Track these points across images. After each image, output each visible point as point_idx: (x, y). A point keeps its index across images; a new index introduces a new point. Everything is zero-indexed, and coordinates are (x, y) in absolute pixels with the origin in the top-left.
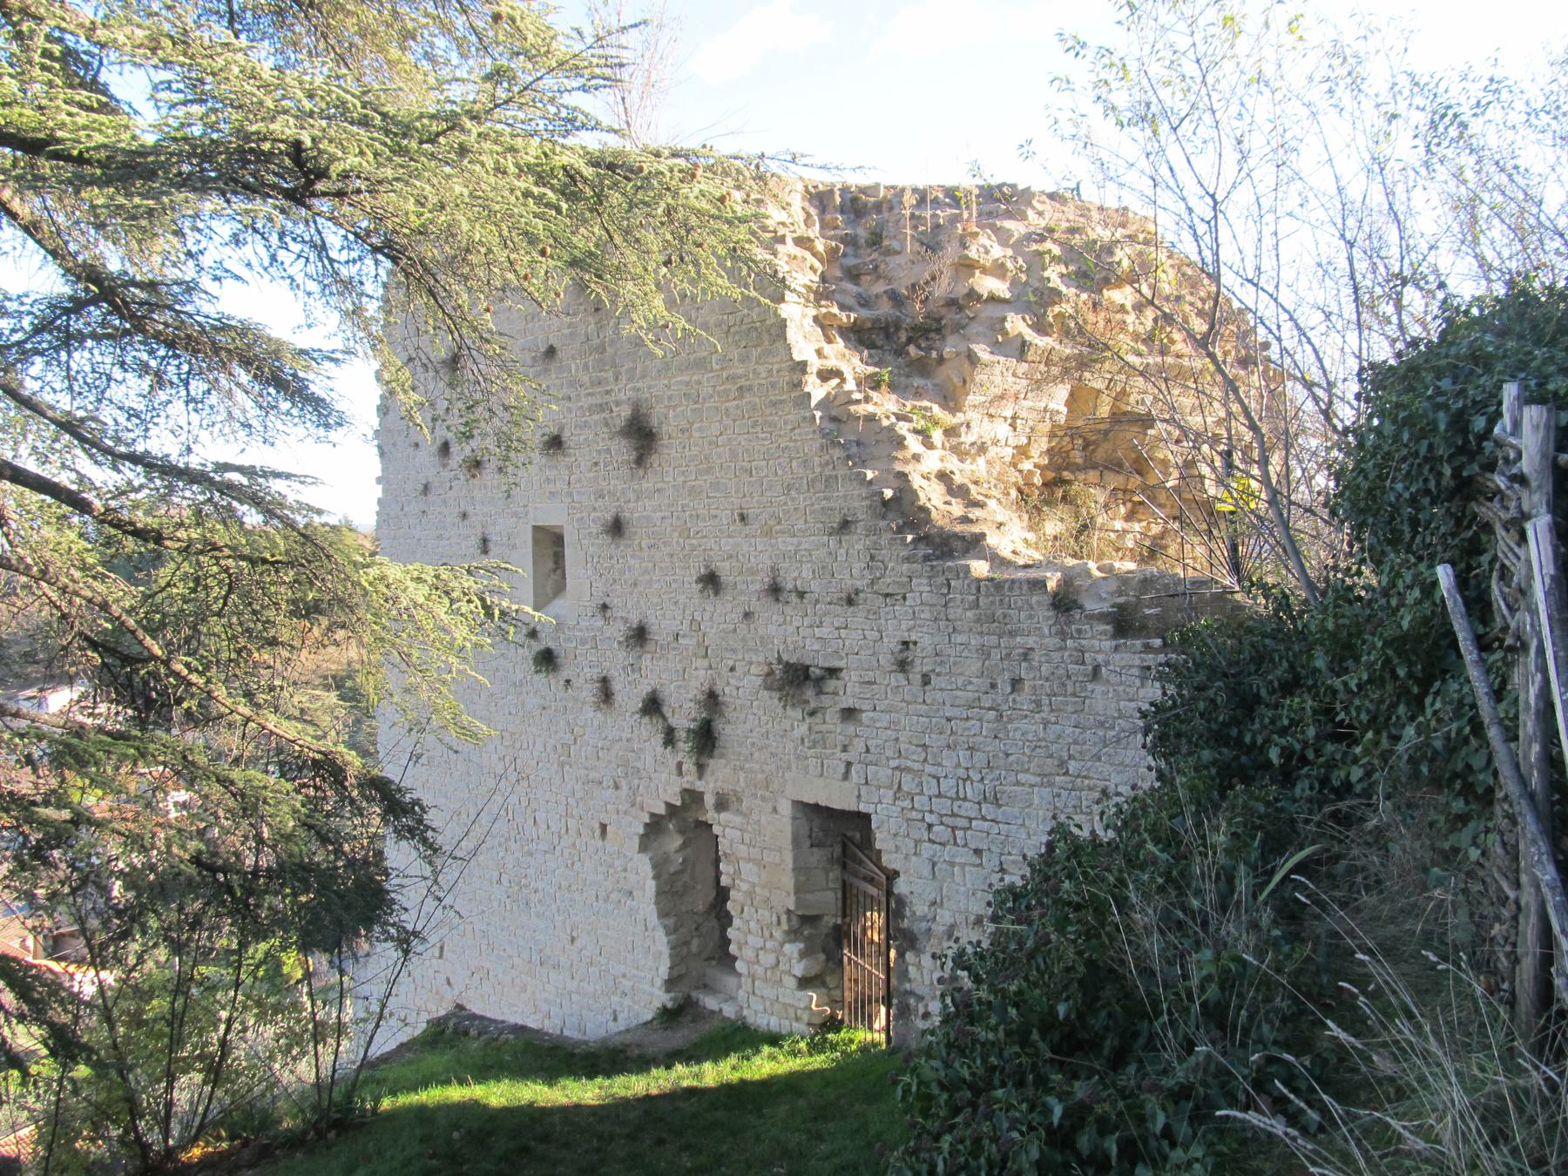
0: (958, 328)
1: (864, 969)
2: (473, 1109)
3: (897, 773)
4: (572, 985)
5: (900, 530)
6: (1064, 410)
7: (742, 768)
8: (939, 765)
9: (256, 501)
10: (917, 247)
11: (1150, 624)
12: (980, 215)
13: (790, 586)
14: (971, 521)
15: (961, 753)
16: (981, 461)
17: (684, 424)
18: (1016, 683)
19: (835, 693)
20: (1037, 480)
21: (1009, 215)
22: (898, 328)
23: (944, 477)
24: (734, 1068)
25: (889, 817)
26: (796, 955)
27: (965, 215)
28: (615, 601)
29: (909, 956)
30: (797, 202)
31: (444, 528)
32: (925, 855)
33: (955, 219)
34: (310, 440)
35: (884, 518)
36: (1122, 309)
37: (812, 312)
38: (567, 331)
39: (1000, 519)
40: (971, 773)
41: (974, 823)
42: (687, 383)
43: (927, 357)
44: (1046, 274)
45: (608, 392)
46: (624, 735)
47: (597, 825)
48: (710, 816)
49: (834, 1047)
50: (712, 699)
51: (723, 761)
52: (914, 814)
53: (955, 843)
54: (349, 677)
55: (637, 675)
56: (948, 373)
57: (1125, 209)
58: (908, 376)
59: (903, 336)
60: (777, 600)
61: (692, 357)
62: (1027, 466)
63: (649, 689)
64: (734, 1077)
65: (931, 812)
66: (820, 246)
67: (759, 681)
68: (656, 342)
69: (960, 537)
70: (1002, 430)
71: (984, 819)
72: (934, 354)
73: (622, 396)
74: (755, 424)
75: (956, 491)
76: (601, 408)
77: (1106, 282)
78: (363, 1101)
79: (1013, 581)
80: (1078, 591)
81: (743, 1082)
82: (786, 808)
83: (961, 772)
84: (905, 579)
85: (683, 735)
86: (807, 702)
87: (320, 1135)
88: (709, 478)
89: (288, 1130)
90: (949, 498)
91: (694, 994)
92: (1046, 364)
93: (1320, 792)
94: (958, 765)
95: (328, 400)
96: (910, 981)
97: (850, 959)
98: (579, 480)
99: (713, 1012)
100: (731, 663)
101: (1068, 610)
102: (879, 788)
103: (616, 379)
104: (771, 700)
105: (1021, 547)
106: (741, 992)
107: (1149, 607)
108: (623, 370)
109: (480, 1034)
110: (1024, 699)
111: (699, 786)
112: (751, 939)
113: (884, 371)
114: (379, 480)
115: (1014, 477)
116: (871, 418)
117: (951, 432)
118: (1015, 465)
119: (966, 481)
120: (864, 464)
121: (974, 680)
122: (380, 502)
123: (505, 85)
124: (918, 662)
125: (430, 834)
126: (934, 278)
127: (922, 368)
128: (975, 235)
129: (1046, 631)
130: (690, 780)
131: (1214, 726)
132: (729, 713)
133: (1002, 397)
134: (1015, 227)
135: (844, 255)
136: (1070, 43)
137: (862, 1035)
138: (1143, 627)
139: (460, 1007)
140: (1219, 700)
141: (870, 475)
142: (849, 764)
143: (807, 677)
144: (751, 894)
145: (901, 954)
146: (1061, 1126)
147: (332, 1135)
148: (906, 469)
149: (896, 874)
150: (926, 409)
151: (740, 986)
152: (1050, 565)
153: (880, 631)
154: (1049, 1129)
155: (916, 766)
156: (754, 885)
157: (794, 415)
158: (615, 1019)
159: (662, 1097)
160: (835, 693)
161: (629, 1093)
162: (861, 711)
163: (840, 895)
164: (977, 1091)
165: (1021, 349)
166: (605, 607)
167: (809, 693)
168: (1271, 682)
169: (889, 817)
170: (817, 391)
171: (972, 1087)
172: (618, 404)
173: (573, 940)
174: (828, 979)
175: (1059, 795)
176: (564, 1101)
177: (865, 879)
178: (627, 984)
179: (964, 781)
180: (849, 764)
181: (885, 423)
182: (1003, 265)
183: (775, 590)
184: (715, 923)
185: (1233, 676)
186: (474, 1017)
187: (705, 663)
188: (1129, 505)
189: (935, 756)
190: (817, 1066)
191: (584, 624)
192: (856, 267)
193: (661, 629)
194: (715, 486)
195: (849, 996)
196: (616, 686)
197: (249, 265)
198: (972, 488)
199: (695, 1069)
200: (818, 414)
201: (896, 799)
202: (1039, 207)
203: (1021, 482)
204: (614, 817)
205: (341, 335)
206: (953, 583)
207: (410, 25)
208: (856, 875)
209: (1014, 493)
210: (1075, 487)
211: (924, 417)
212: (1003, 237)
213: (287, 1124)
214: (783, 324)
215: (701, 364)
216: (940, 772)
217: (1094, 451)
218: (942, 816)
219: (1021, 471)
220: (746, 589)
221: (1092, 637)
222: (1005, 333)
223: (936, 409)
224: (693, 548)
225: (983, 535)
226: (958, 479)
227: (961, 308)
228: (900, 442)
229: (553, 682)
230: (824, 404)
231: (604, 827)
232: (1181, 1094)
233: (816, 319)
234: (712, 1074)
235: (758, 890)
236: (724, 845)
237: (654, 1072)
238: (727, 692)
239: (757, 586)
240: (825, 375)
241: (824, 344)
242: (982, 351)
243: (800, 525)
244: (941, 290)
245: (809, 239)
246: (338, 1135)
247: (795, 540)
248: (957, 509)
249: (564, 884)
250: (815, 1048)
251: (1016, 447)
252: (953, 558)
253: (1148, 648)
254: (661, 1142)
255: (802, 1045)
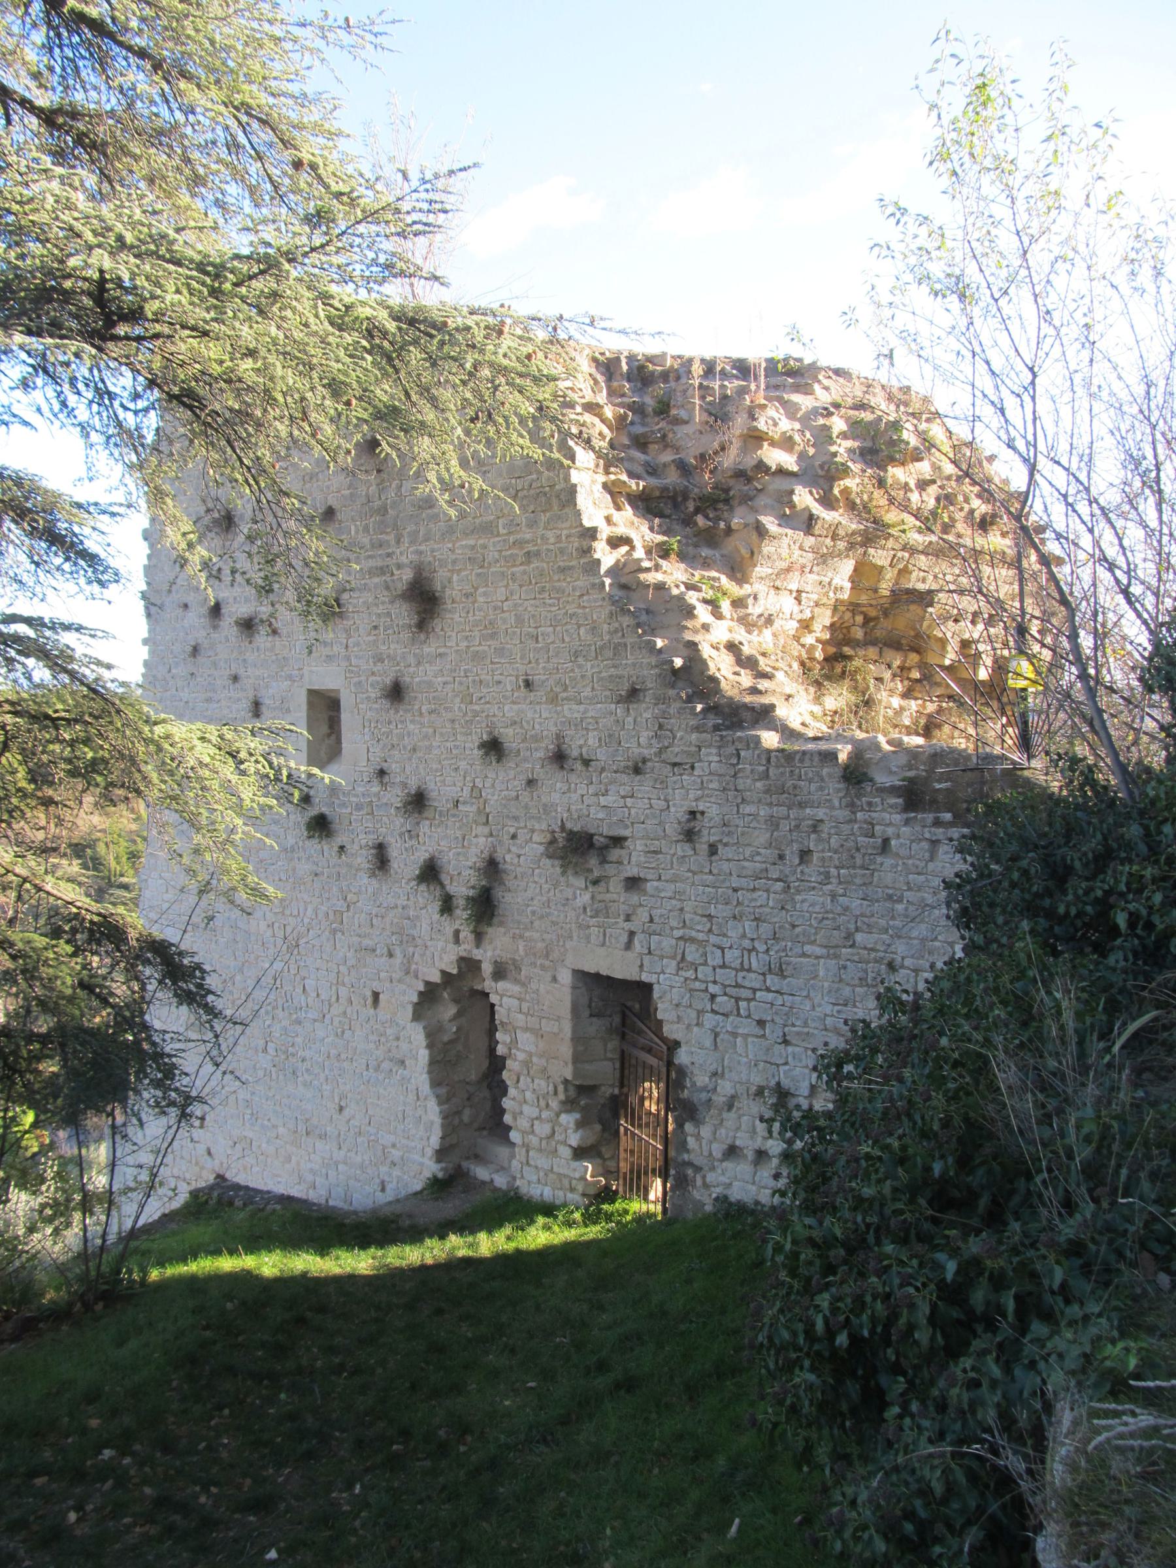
0: (746, 499)
1: (641, 1139)
2: (246, 1278)
3: (682, 943)
4: (339, 1155)
5: (690, 699)
6: (848, 585)
7: (521, 937)
8: (725, 935)
9: (43, 654)
10: (705, 416)
11: (940, 797)
12: (767, 387)
13: (575, 753)
14: (760, 692)
15: (747, 924)
16: (767, 633)
17: (468, 589)
18: (805, 855)
19: (620, 863)
20: (819, 655)
21: (797, 388)
22: (686, 498)
23: (732, 647)
24: (509, 1238)
25: (672, 987)
26: (572, 1125)
27: (753, 387)
28: (393, 767)
29: (688, 1127)
30: (586, 366)
31: (215, 691)
32: (707, 1025)
33: (743, 391)
34: (81, 597)
35: (673, 687)
36: (906, 487)
37: (601, 478)
38: (347, 492)
39: (788, 691)
40: (756, 944)
41: (758, 994)
42: (473, 547)
43: (716, 527)
44: (833, 449)
45: (389, 555)
46: (399, 902)
47: (369, 994)
48: (488, 985)
49: (609, 1217)
50: (492, 867)
51: (502, 930)
52: (697, 985)
53: (739, 1015)
54: (89, 846)
55: (414, 842)
56: (737, 544)
57: (908, 388)
58: (696, 546)
59: (691, 506)
60: (562, 767)
61: (477, 521)
62: (809, 640)
63: (427, 855)
64: (510, 1247)
65: (715, 982)
66: (609, 412)
67: (541, 849)
68: (450, 503)
69: (750, 708)
70: (787, 603)
71: (768, 990)
72: (722, 525)
73: (404, 559)
74: (543, 590)
75: (746, 662)
76: (382, 571)
77: (892, 460)
78: (130, 1272)
79: (804, 753)
80: (868, 763)
81: (518, 1251)
82: (565, 977)
83: (746, 943)
84: (693, 749)
85: (462, 902)
86: (590, 871)
87: (87, 1307)
88: (494, 643)
89: (52, 1301)
90: (738, 669)
91: (465, 1164)
92: (833, 539)
93: (1134, 963)
94: (744, 936)
95: (103, 555)
96: (688, 1151)
97: (626, 1129)
98: (358, 644)
99: (483, 1183)
100: (512, 830)
101: (859, 782)
102: (662, 957)
103: (398, 542)
104: (552, 868)
105: (808, 720)
106: (515, 1163)
107: (940, 782)
108: (405, 533)
109: (245, 1205)
110: (812, 873)
111: (477, 954)
112: (526, 1109)
113: (673, 540)
114: (145, 642)
115: (796, 650)
116: (661, 587)
117: (738, 603)
118: (797, 638)
119: (754, 652)
120: (653, 632)
121: (763, 851)
122: (146, 664)
123: (324, 228)
124: (705, 832)
125: (210, 998)
126: (723, 449)
127: (710, 538)
128: (763, 407)
129: (836, 803)
130: (467, 947)
131: (1027, 896)
132: (510, 883)
133: (788, 570)
134: (804, 402)
135: (632, 423)
136: (891, 210)
137: (636, 1206)
138: (934, 801)
139: (220, 1177)
140: (1033, 871)
141: (660, 643)
142: (632, 934)
143: (591, 845)
144: (527, 1064)
145: (680, 1125)
146: (953, 1280)
147: (99, 1306)
148: (696, 638)
149: (677, 1044)
150: (714, 579)
151: (513, 1156)
152: (839, 738)
153: (666, 800)
154: (942, 1285)
155: (701, 936)
156: (530, 1055)
157: (582, 582)
158: (383, 1190)
159: (437, 1267)
160: (620, 863)
161: (404, 1263)
162: (646, 880)
163: (618, 1065)
164: (851, 1251)
165: (808, 523)
166: (382, 773)
167: (593, 862)
168: (1085, 854)
169: (672, 987)
170: (607, 557)
171: (844, 1244)
172: (399, 567)
173: (341, 1109)
174: (603, 1150)
175: (845, 967)
176: (337, 1270)
177: (643, 1049)
178: (396, 1154)
179: (750, 951)
180: (632, 934)
181: (675, 592)
182: (791, 438)
183: (559, 758)
184: (486, 1093)
185: (1044, 847)
186: (237, 1187)
187: (486, 830)
188: (906, 683)
189: (720, 926)
190: (591, 1236)
191: (360, 789)
192: (644, 435)
193: (442, 791)
194: (500, 651)
195: (624, 1167)
196: (393, 853)
197: (39, 410)
198: (761, 659)
199: (470, 1239)
200: (608, 581)
201: (679, 969)
202: (826, 382)
203: (804, 656)
204: (388, 985)
205: (123, 488)
206: (742, 753)
207: (201, 171)
208: (635, 1046)
209: (796, 665)
210: (857, 663)
211: (712, 587)
212: (791, 410)
213: (50, 1295)
214: (572, 490)
215: (488, 529)
216: (726, 943)
217: (874, 627)
218: (725, 986)
219: (803, 646)
220: (534, 760)
221: (883, 810)
222: (792, 506)
223: (724, 580)
224: (476, 714)
225: (772, 707)
226: (746, 650)
227: (749, 480)
228: (690, 612)
229: (326, 848)
230: (613, 571)
231: (376, 996)
232: (1075, 1249)
233: (605, 486)
234: (487, 1244)
235: (535, 1059)
236: (501, 1014)
237: (428, 1242)
238: (508, 859)
239: (540, 754)
240: (615, 542)
241: (612, 511)
242: (770, 523)
243: (587, 692)
244: (729, 460)
245: (598, 405)
246: (105, 1307)
247: (582, 708)
248: (746, 679)
249: (333, 1052)
250: (590, 1218)
251: (799, 621)
252: (742, 728)
253: (937, 823)
254: (439, 1312)
255: (577, 1216)
